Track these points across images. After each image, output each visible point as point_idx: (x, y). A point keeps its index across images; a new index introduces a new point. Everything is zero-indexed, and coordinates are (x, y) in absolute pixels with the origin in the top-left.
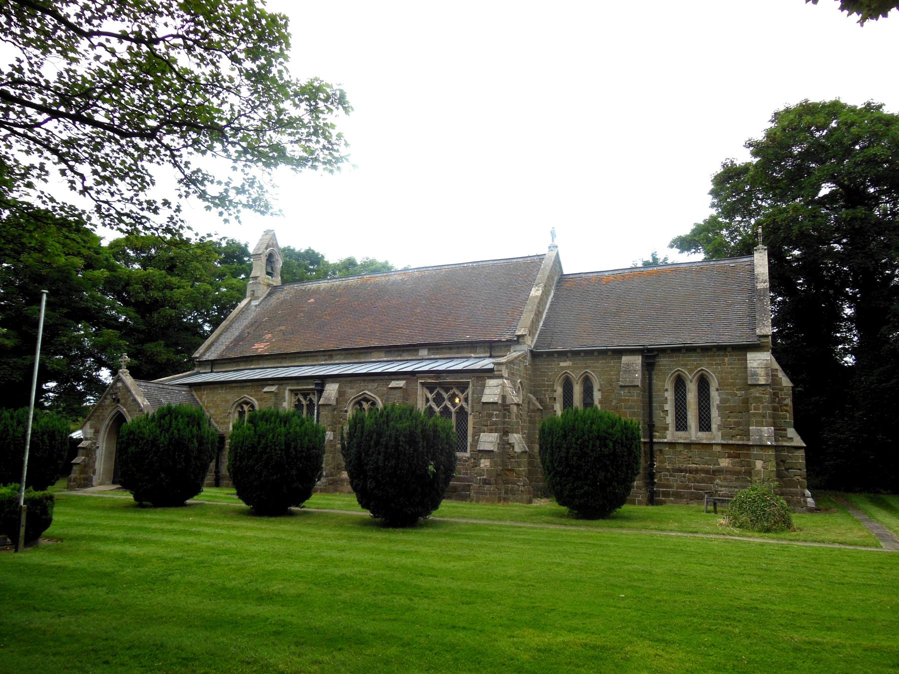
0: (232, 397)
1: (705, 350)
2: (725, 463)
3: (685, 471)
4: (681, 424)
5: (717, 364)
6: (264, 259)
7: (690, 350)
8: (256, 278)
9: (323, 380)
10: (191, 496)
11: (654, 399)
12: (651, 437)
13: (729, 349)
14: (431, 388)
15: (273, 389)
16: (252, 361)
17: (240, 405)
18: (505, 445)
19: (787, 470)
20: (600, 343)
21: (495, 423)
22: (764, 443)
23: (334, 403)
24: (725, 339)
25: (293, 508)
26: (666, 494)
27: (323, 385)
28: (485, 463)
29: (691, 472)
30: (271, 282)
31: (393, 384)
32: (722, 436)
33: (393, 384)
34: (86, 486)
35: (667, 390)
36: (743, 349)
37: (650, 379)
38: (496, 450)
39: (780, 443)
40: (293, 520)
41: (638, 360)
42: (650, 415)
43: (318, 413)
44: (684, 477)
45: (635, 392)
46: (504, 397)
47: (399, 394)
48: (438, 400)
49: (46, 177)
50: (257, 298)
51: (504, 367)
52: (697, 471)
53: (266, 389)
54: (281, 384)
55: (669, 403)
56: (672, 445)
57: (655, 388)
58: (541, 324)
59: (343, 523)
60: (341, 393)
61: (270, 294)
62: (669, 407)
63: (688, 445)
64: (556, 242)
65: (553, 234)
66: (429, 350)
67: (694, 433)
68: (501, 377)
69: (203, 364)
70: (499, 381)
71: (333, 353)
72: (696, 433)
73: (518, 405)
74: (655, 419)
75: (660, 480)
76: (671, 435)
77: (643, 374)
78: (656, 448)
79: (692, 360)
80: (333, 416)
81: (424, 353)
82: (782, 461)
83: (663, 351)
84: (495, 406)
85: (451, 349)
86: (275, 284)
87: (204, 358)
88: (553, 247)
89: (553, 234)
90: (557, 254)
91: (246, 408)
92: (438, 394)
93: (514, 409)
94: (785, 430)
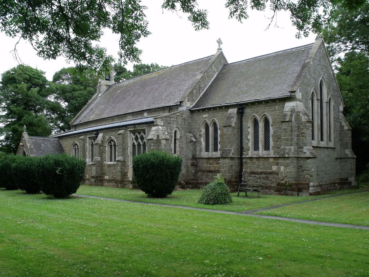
1: (267, 102)
4: (256, 148)
5: (272, 111)
7: (259, 102)
9: (97, 132)
11: (244, 133)
12: (241, 154)
13: (277, 101)
14: (134, 132)
16: (88, 124)
19: (303, 171)
22: (284, 156)
23: (100, 143)
26: (201, 183)
29: (258, 174)
30: (108, 84)
32: (274, 153)
35: (249, 127)
39: (299, 156)
41: (235, 110)
44: (255, 177)
45: (230, 129)
46: (158, 136)
48: (137, 139)
49: (303, 36)
52: (261, 173)
53: (80, 138)
54: (86, 135)
55: (250, 135)
56: (251, 158)
60: (104, 137)
62: (250, 137)
63: (258, 158)
65: (219, 42)
66: (148, 113)
67: (261, 152)
68: (157, 125)
71: (114, 118)
72: (262, 151)
74: (244, 144)
75: (245, 178)
77: (237, 118)
78: (244, 160)
80: (100, 149)
82: (301, 166)
84: (152, 141)
85: (155, 111)
89: (219, 42)
92: (137, 136)
94: (302, 148)
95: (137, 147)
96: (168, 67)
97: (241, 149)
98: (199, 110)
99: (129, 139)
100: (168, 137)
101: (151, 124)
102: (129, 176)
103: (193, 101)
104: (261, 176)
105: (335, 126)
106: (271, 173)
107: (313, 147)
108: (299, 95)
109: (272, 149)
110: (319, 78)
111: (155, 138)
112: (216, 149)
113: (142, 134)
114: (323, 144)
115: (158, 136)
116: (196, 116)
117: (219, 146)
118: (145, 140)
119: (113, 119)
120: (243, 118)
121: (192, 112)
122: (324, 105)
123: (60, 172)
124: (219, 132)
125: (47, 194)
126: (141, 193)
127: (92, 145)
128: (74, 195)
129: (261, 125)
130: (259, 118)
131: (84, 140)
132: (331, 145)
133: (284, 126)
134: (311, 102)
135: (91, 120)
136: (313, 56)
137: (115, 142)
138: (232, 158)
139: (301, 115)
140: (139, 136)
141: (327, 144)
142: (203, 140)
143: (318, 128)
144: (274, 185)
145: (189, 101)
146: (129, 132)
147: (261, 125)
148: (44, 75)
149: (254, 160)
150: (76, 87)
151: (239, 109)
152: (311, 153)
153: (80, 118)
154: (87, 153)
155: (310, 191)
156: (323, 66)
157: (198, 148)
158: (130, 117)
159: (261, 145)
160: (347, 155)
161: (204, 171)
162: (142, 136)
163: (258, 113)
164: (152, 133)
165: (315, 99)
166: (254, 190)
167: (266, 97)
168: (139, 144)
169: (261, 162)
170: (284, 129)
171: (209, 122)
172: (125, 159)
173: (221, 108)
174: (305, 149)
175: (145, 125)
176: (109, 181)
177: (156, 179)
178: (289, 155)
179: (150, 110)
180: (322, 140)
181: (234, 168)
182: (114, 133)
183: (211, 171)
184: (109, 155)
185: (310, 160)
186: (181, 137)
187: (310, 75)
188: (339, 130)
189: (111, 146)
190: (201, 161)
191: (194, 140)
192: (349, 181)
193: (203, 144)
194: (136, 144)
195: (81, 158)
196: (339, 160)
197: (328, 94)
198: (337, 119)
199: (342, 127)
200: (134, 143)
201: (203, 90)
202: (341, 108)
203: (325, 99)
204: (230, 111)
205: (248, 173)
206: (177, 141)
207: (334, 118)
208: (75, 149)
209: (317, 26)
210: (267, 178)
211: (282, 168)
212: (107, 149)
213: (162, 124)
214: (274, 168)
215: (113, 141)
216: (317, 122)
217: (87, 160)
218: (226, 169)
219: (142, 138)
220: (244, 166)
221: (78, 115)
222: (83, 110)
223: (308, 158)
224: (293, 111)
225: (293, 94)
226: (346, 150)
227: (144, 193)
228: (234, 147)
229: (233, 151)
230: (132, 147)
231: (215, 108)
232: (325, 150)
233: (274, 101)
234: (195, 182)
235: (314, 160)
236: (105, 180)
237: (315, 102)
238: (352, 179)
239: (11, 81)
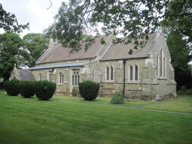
1: (137, 58)
4: (131, 79)
5: (139, 62)
8: (51, 43)
9: (53, 69)
12: (124, 82)
17: (60, 74)
23: (55, 74)
25: (31, 97)
26: (105, 95)
27: (54, 70)
29: (132, 91)
33: (44, 71)
41: (122, 61)
43: (52, 77)
45: (119, 70)
48: (75, 73)
50: (51, 48)
52: (134, 90)
58: (105, 53)
60: (57, 71)
61: (54, 46)
62: (129, 74)
67: (134, 81)
68: (86, 67)
70: (85, 68)
76: (129, 81)
78: (125, 85)
81: (77, 61)
83: (127, 59)
85: (82, 60)
86: (56, 44)
87: (37, 63)
91: (62, 74)
92: (75, 72)
94: (153, 80)
95: (75, 77)
98: (104, 61)
99: (71, 73)
100: (90, 73)
103: (101, 56)
104: (134, 92)
105: (167, 69)
106: (138, 91)
107: (158, 79)
108: (151, 56)
109: (139, 80)
110: (160, 48)
113: (78, 71)
114: (162, 78)
115: (86, 72)
117: (114, 78)
118: (79, 74)
119: (60, 62)
120: (126, 65)
122: (162, 60)
123: (46, 89)
124: (114, 71)
125: (39, 98)
126: (83, 98)
127: (50, 75)
128: (51, 99)
129: (134, 69)
130: (133, 66)
132: (165, 78)
133: (145, 70)
134: (156, 59)
135: (47, 62)
136: (158, 38)
137: (63, 74)
138: (120, 84)
139: (152, 65)
140: (76, 72)
141: (164, 77)
143: (159, 70)
144: (139, 96)
145: (99, 56)
146: (71, 70)
149: (130, 85)
150: (35, 43)
151: (123, 61)
152: (157, 82)
155: (157, 99)
156: (162, 42)
157: (103, 78)
158: (69, 62)
160: (172, 82)
161: (106, 89)
162: (78, 72)
163: (133, 63)
164: (83, 71)
165: (158, 57)
166: (132, 98)
168: (76, 76)
169: (134, 85)
170: (145, 71)
171: (109, 66)
173: (115, 60)
174: (154, 80)
176: (59, 92)
178: (147, 83)
179: (80, 59)
180: (161, 76)
181: (121, 88)
182: (63, 70)
183: (109, 89)
184: (60, 80)
185: (156, 85)
186: (95, 73)
187: (156, 47)
188: (169, 71)
189: (61, 76)
190: (105, 84)
191: (102, 74)
192: (173, 95)
193: (106, 76)
194: (74, 75)
195: (54, 81)
196: (169, 85)
197: (164, 55)
198: (168, 66)
199: (170, 70)
200: (73, 75)
201: (106, 51)
202: (170, 61)
203: (163, 57)
204: (119, 61)
205: (127, 90)
206: (94, 75)
207: (167, 65)
208: (40, 76)
210: (136, 93)
211: (144, 89)
212: (59, 77)
213: (88, 67)
214: (140, 88)
216: (159, 68)
219: (78, 73)
220: (126, 87)
221: (39, 59)
222: (45, 58)
223: (155, 84)
224: (149, 63)
225: (149, 56)
226: (172, 80)
227: (83, 98)
228: (121, 78)
229: (121, 80)
230: (72, 77)
231: (112, 60)
232: (162, 80)
234: (102, 94)
235: (158, 85)
236: (57, 92)
237: (158, 59)
238: (175, 94)
239: (3, 40)
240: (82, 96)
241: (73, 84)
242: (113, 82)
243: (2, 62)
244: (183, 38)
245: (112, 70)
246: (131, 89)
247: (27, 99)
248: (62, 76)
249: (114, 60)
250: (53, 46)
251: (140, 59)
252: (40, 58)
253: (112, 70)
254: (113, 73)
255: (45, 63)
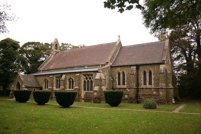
0: (43, 78)
1: (151, 64)
2: (155, 93)
3: (145, 95)
4: (145, 84)
6: (55, 46)
8: (52, 50)
9: (62, 74)
10: (27, 101)
12: (138, 87)
15: (52, 76)
17: (70, 79)
18: (101, 89)
20: (126, 64)
21: (98, 84)
24: (155, 62)
28: (95, 94)
31: (77, 75)
33: (77, 75)
34: (12, 98)
36: (159, 64)
37: (138, 72)
38: (98, 90)
40: (45, 106)
41: (135, 67)
42: (138, 82)
45: (134, 76)
46: (101, 78)
47: (78, 77)
48: (87, 78)
51: (101, 70)
52: (148, 95)
57: (139, 75)
59: (56, 107)
60: (66, 77)
61: (56, 54)
62: (142, 79)
63: (146, 89)
64: (120, 39)
65: (119, 37)
67: (148, 86)
68: (100, 72)
69: (40, 71)
73: (104, 79)
76: (143, 86)
79: (148, 67)
83: (141, 65)
88: (119, 40)
89: (119, 37)
90: (120, 41)
91: (71, 80)
92: (87, 77)
93: (103, 80)
96: (78, 47)
97: (138, 85)
98: (115, 66)
101: (97, 72)
102: (82, 96)
111: (99, 79)
112: (124, 84)
115: (101, 78)
116: (113, 69)
117: (126, 83)
121: (111, 67)
124: (126, 77)
129: (147, 74)
131: (53, 78)
137: (48, 81)
138: (135, 88)
139: (167, 70)
140: (88, 77)
142: (117, 80)
147: (147, 74)
148: (19, 44)
149: (144, 89)
153: (44, 67)
154: (54, 84)
159: (147, 83)
160: (176, 87)
163: (147, 69)
167: (130, 63)
169: (148, 90)
171: (121, 72)
172: (79, 88)
173: (127, 66)
175: (93, 72)
177: (113, 99)
189: (70, 82)
204: (132, 67)
209: (165, 31)
212: (68, 83)
215: (71, 79)
217: (54, 88)
218: (132, 93)
219: (90, 78)
222: (50, 63)
229: (134, 85)
231: (124, 66)
233: (154, 64)
240: (107, 102)
241: (85, 90)
242: (126, 87)
243: (2, 68)
244: (192, 44)
245: (124, 76)
246: (145, 94)
247: (65, 109)
248: (47, 82)
249: (126, 66)
250: (55, 53)
251: (154, 65)
252: (43, 63)
253: (124, 76)
254: (126, 78)
255: (49, 70)
